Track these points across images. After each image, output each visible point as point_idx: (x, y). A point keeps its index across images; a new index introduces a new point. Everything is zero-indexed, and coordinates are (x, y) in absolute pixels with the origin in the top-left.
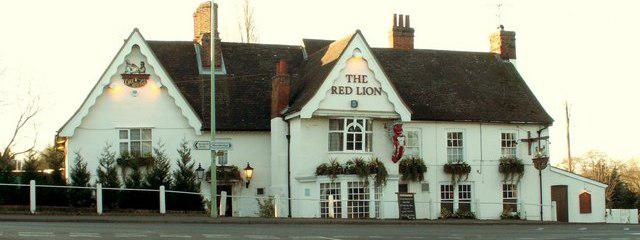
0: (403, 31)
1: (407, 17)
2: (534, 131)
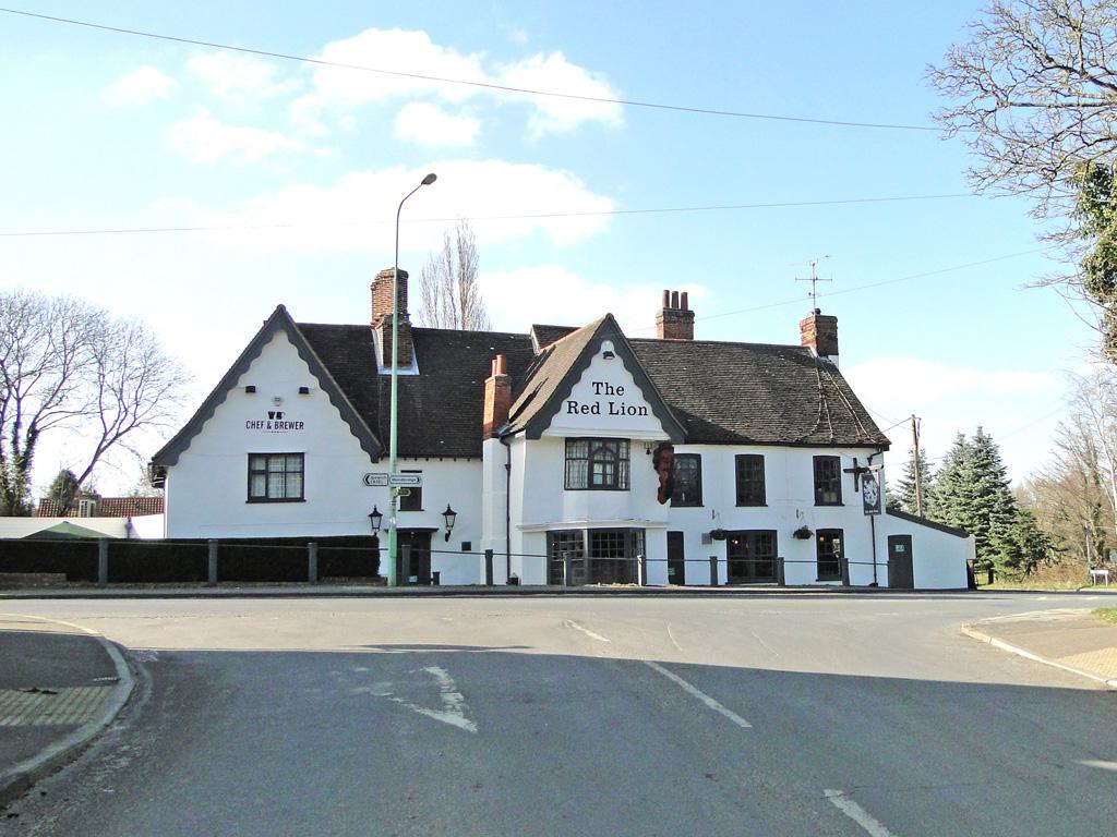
0: (677, 314)
1: (685, 296)
2: (862, 456)
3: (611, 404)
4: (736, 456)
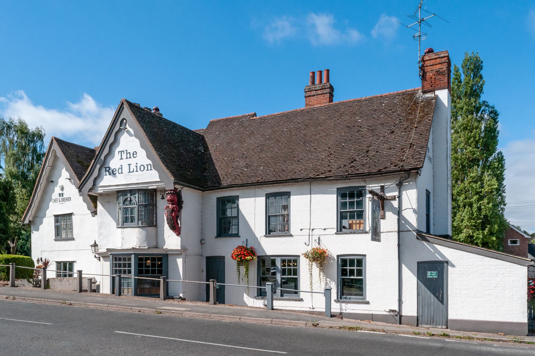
3: (129, 165)
4: (218, 198)
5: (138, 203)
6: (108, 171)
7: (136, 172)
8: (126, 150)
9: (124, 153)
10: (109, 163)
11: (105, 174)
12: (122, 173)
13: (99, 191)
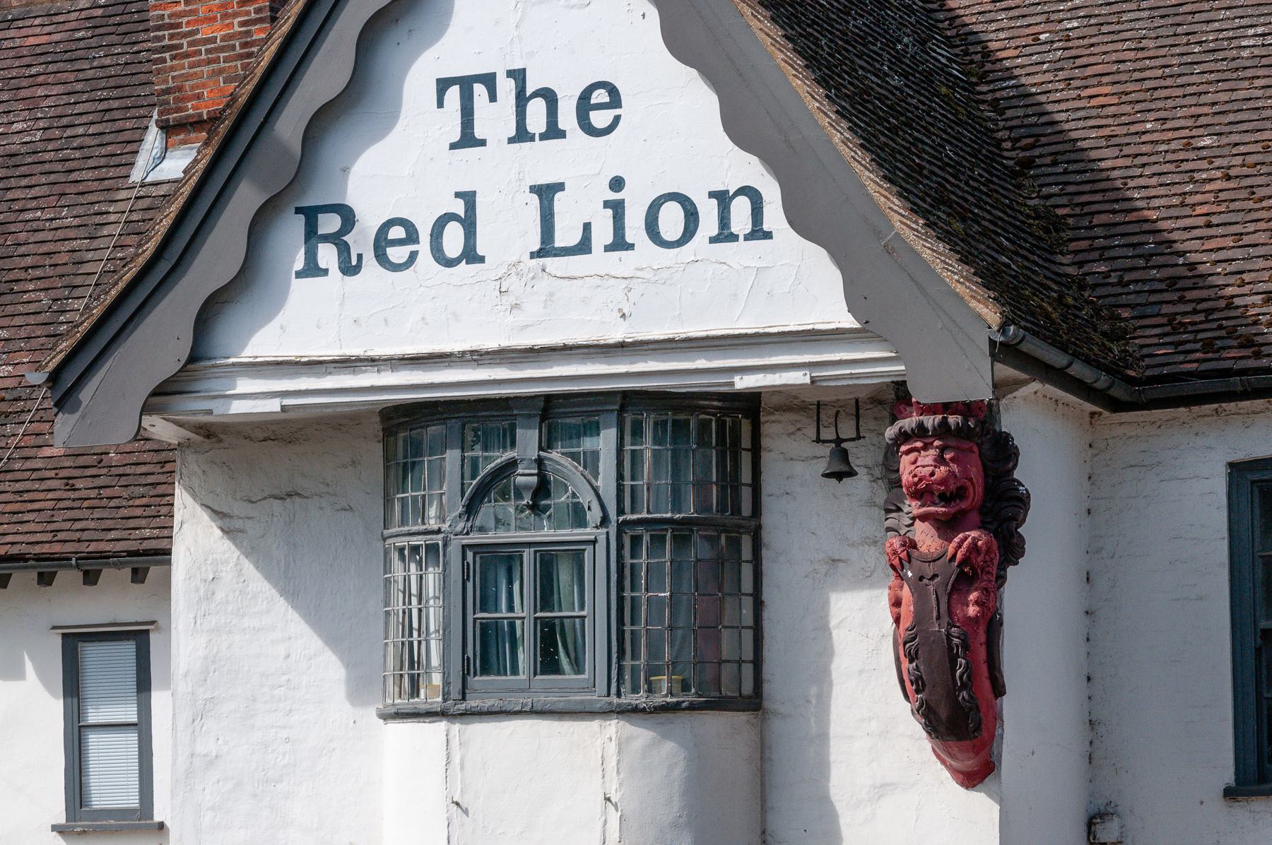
3: (546, 193)
4: (1237, 470)
5: (620, 511)
6: (336, 239)
7: (608, 248)
8: (511, 74)
9: (493, 97)
10: (346, 170)
11: (299, 264)
12: (471, 255)
13: (238, 407)
